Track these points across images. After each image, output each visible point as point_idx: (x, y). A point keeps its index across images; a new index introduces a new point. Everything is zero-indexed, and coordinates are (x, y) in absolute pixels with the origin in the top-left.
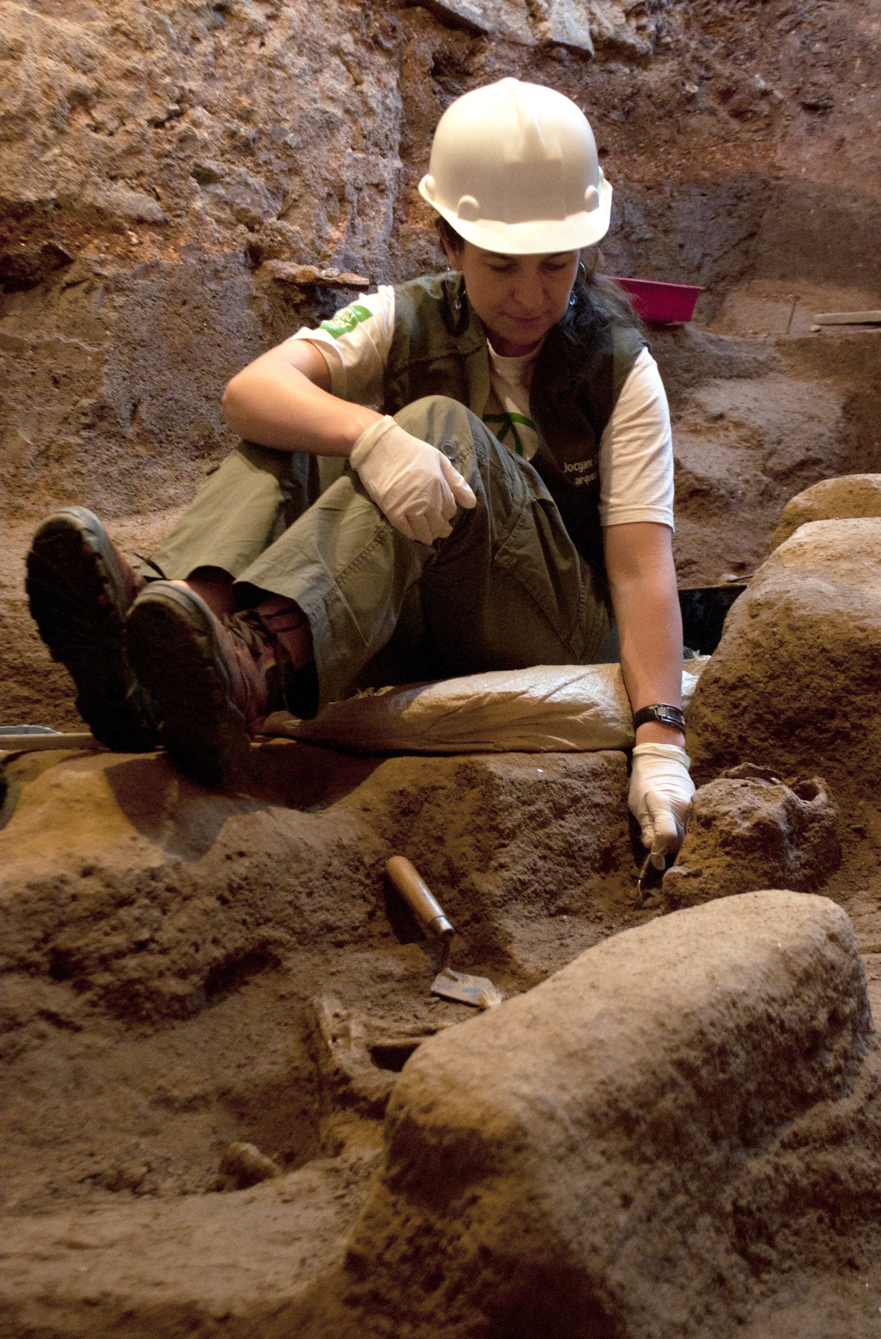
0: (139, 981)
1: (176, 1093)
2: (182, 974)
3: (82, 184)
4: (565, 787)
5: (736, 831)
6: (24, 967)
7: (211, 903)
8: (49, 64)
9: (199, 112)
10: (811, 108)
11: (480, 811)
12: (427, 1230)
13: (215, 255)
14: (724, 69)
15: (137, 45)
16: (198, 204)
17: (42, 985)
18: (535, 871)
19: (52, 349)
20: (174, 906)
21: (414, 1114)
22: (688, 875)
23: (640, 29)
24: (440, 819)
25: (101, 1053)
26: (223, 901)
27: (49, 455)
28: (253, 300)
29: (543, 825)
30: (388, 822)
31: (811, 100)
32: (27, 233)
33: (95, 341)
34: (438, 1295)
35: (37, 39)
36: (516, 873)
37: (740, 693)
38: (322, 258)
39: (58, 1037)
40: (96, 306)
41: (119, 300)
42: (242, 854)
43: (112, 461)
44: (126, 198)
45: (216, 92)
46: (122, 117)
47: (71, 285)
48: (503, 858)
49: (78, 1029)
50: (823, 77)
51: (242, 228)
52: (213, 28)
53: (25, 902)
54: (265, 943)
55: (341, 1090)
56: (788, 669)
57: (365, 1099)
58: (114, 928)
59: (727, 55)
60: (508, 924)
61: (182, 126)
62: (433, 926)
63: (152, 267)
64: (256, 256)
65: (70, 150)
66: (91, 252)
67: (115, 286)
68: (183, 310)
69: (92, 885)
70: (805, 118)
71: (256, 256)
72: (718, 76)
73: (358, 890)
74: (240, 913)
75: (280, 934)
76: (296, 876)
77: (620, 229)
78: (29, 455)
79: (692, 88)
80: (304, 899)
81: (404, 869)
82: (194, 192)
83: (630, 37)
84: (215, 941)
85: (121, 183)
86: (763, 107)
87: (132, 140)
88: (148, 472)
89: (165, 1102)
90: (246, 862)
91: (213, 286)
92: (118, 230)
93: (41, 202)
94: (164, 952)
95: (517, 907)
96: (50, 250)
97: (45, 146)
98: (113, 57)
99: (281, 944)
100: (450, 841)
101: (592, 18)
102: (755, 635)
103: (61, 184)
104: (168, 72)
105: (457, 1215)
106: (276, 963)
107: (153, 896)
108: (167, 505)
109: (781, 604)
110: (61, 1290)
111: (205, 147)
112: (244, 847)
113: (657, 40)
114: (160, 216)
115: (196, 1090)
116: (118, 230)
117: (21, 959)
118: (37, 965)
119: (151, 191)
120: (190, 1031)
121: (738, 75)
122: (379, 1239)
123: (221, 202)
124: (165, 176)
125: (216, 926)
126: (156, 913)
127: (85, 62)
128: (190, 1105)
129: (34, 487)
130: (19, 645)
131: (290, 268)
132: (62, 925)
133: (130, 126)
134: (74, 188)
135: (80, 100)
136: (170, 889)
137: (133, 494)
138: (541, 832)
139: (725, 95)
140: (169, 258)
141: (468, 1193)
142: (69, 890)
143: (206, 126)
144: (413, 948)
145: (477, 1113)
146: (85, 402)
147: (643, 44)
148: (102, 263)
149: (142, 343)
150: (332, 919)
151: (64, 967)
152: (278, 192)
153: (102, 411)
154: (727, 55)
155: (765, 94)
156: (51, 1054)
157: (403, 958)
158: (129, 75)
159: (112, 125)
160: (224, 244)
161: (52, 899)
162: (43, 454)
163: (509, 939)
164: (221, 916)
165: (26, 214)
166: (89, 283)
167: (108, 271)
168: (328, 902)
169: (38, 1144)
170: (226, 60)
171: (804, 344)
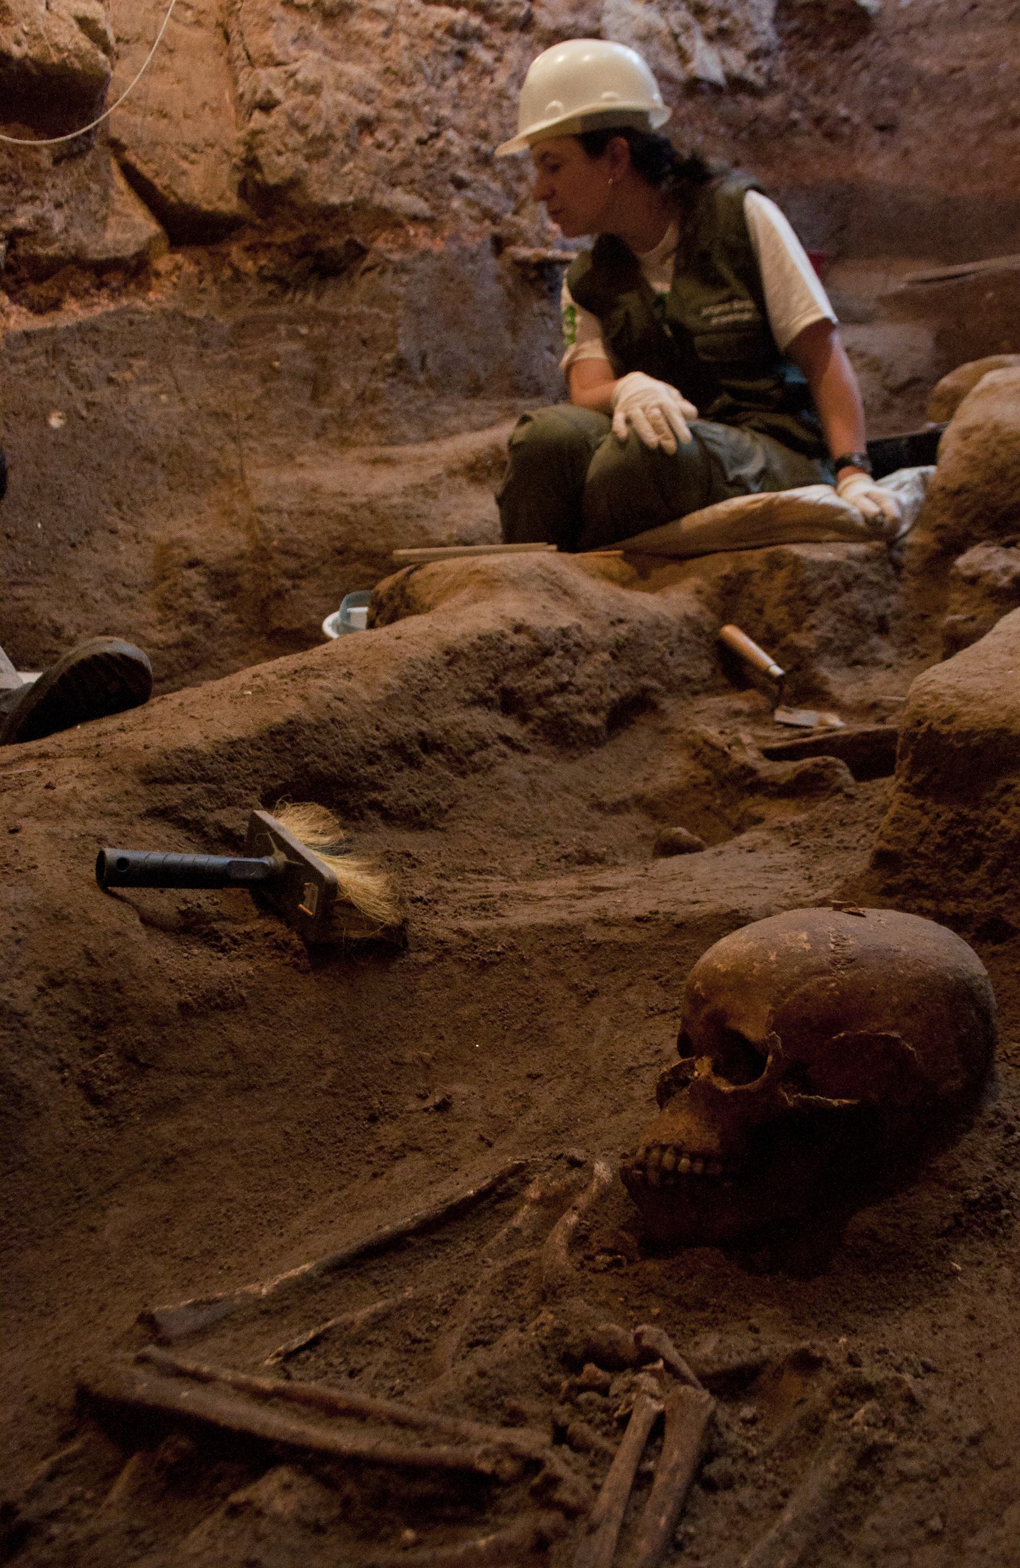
0: (565, 714)
1: (605, 799)
2: (594, 711)
3: (372, 191)
4: (850, 567)
5: (1000, 584)
6: (482, 701)
7: (606, 656)
8: (342, 97)
9: (451, 134)
10: (882, 128)
11: (790, 587)
12: (962, 820)
13: (472, 244)
14: (816, 101)
15: (403, 82)
16: (456, 204)
17: (496, 715)
18: (836, 630)
19: (360, 319)
20: (581, 658)
21: (936, 726)
22: (966, 621)
23: (758, 70)
24: (758, 595)
25: (545, 771)
26: (614, 656)
27: (364, 398)
28: (499, 278)
29: (838, 595)
30: (716, 600)
31: (881, 121)
32: (335, 229)
33: (390, 310)
34: (980, 873)
35: (331, 79)
36: (822, 632)
37: (963, 497)
38: (546, 245)
39: (516, 757)
40: (389, 284)
41: (405, 278)
42: (621, 621)
43: (410, 401)
44: (404, 200)
45: (462, 118)
46: (397, 137)
47: (369, 269)
48: (812, 620)
49: (526, 752)
50: (889, 103)
51: (487, 223)
52: (457, 69)
53: (479, 650)
54: (645, 690)
55: (748, 781)
56: (1001, 474)
57: (774, 784)
58: (543, 673)
59: (817, 91)
60: (824, 671)
61: (440, 144)
62: (767, 674)
63: (425, 254)
64: (499, 244)
65: (362, 164)
66: (382, 244)
67: (401, 269)
68: (452, 285)
69: (522, 640)
70: (876, 137)
71: (499, 244)
72: (812, 107)
73: (703, 652)
74: (627, 666)
75: (654, 683)
76: (661, 639)
77: (319, 628)
78: (351, 398)
79: (795, 115)
80: (668, 657)
81: (733, 633)
82: (450, 197)
83: (750, 75)
84: (612, 687)
85: (399, 189)
86: (846, 130)
87: (406, 154)
88: (436, 408)
89: (600, 806)
90: (626, 627)
91: (470, 266)
92: (399, 225)
93: (343, 205)
94: (579, 692)
95: (827, 658)
96: (351, 243)
97: (344, 161)
98: (386, 91)
99: (655, 691)
100: (768, 610)
101: (723, 61)
102: (969, 451)
103: (356, 191)
104: (427, 102)
105: (990, 803)
106: (654, 707)
107: (566, 650)
108: (452, 433)
109: (990, 425)
110: (611, 914)
111: (457, 160)
112: (622, 615)
113: (769, 77)
114: (428, 213)
115: (619, 797)
116: (399, 225)
117: (481, 695)
118: (492, 700)
119: (421, 195)
120: (603, 756)
121: (827, 106)
122: (910, 836)
123: (470, 203)
124: (430, 182)
125: (612, 675)
126: (570, 663)
127: (367, 96)
128: (618, 808)
129: (356, 422)
130: (361, 536)
131: (524, 252)
132: (506, 669)
133: (403, 144)
134: (367, 195)
135: (366, 125)
136: (577, 645)
137: (428, 426)
138: (836, 601)
139: (818, 121)
140: (438, 246)
141: (1000, 784)
142: (508, 642)
143: (458, 145)
144: (752, 692)
145: (1002, 716)
146: (388, 357)
147: (760, 81)
148: (390, 251)
149: (424, 310)
150: (688, 673)
151: (510, 703)
152: (511, 195)
153: (400, 363)
154: (817, 91)
155: (846, 120)
156: (512, 768)
157: (747, 700)
158: (399, 105)
159: (390, 143)
160: (475, 236)
161: (498, 649)
162: (361, 397)
163: (825, 681)
164: (613, 668)
165: (332, 215)
166: (383, 266)
167: (396, 257)
168: (683, 659)
169: (516, 836)
170: (466, 94)
171: (898, 298)
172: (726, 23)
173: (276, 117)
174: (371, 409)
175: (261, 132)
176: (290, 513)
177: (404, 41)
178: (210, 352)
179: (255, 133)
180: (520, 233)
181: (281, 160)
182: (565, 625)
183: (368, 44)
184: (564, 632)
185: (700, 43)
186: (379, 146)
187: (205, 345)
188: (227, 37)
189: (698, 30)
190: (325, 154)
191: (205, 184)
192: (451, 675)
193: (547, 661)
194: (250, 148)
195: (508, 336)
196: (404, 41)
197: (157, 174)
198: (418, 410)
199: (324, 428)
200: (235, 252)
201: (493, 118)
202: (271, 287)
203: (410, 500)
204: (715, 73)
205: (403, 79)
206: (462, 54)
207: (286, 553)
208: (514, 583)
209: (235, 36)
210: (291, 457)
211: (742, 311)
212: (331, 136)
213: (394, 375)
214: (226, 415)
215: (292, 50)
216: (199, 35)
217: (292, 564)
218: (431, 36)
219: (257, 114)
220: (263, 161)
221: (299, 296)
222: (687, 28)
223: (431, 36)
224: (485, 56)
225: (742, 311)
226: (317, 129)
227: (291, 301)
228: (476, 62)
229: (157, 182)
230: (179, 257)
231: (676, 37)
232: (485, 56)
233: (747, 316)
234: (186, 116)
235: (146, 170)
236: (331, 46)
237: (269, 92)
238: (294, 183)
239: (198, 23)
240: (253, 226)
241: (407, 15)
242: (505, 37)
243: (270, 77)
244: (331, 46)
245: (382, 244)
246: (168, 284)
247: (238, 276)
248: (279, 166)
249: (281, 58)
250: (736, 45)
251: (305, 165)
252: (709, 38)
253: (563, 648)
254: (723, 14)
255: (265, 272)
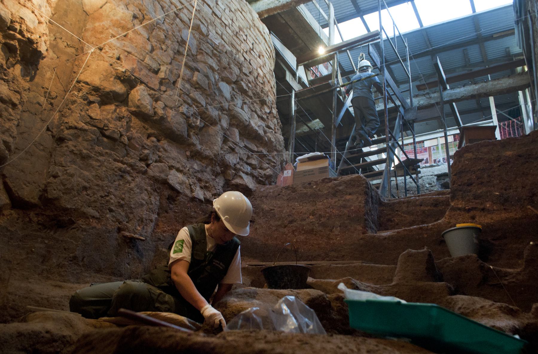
8: (80, 179)
9: (112, 196)
15: (101, 180)
20: (67, 345)
27: (59, 266)
41: (85, 233)
45: (117, 193)
46: (94, 194)
51: (117, 223)
52: (119, 180)
61: (108, 198)
64: (119, 230)
65: (80, 198)
66: (81, 222)
67: (84, 230)
69: (48, 336)
88: (84, 274)
92: (88, 218)
93: (71, 208)
96: (70, 220)
97: (75, 197)
98: (95, 181)
101: (205, 194)
103: (76, 205)
104: (107, 186)
107: (63, 342)
111: (112, 204)
119: (97, 211)
124: (101, 208)
127: (88, 181)
131: (127, 234)
133: (95, 196)
134: (79, 207)
135: (85, 188)
136: (67, 341)
140: (99, 226)
142: (42, 335)
143: (113, 200)
148: (82, 225)
152: (127, 217)
153: (75, 258)
158: (98, 185)
160: (112, 226)
162: (58, 266)
172: (207, 185)
173: (56, 180)
174: (60, 270)
175: (51, 183)
176: (19, 296)
177: (104, 169)
178: (12, 241)
179: (49, 183)
180: (127, 228)
181: (55, 192)
182: (65, 334)
183: (93, 167)
184: (64, 337)
185: (198, 188)
186: (88, 195)
187: (11, 239)
188: (51, 156)
189: (198, 185)
190: (69, 193)
191: (29, 193)
192: (17, 340)
193: (54, 343)
194: (46, 186)
195: (114, 257)
196: (104, 169)
197: (14, 187)
198: (77, 273)
199: (42, 272)
200: (32, 214)
201: (127, 195)
202: (40, 226)
203: (63, 300)
204: (202, 197)
205: (101, 179)
206: (122, 176)
207: (12, 308)
208: (54, 319)
209: (53, 156)
210: (28, 279)
211: (221, 266)
212: (73, 189)
213: (71, 261)
214: (10, 261)
215: (69, 164)
216: (42, 153)
217: (13, 313)
218: (113, 170)
219: (51, 178)
220: (48, 191)
221: (49, 231)
222: (194, 184)
223: (113, 170)
224: (129, 178)
225: (221, 266)
226: (69, 186)
227: (45, 232)
228: (125, 179)
229: (13, 189)
230: (12, 211)
231: (191, 185)
232: (129, 178)
233: (221, 268)
234: (30, 173)
235: (11, 185)
236: (81, 165)
237: (57, 173)
238: (57, 199)
239: (43, 150)
240: (40, 208)
241: (108, 163)
242: (137, 175)
243: (59, 170)
244: (81, 165)
245: (81, 222)
246: (6, 218)
247: (30, 221)
248: (53, 193)
249: (64, 165)
250: (210, 191)
251: (62, 195)
252: (201, 188)
253: (62, 341)
254: (206, 182)
255: (40, 222)
